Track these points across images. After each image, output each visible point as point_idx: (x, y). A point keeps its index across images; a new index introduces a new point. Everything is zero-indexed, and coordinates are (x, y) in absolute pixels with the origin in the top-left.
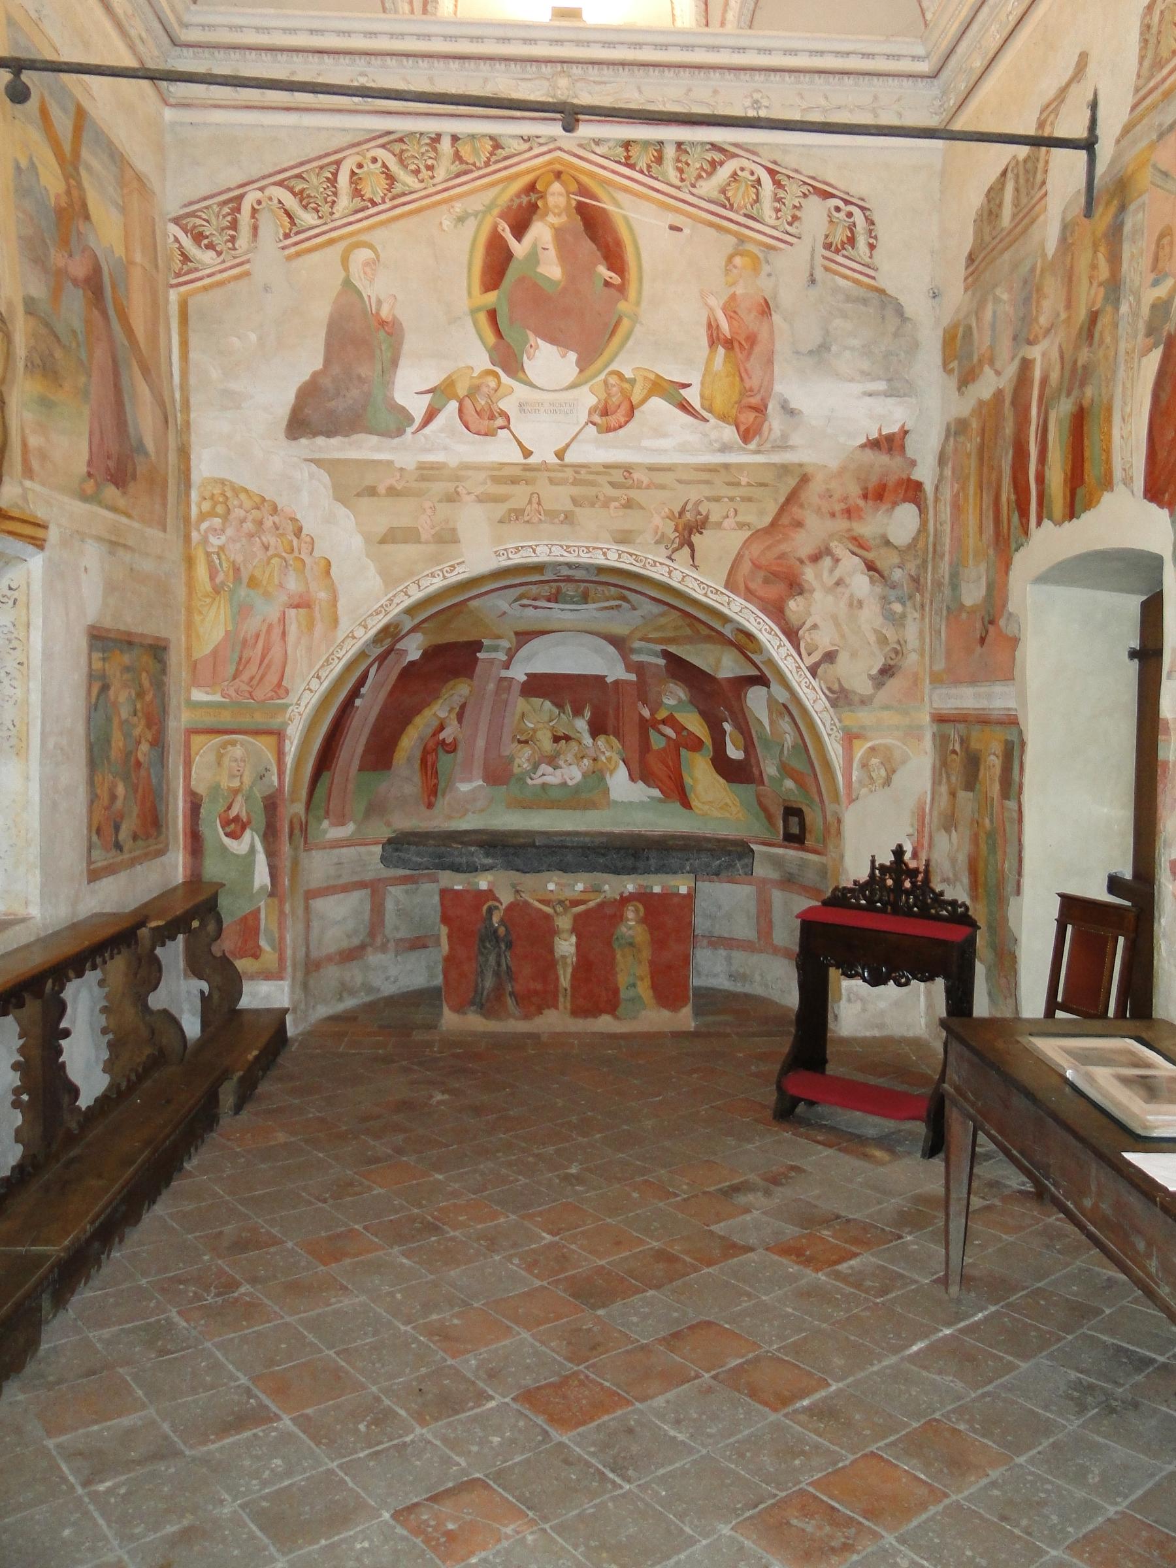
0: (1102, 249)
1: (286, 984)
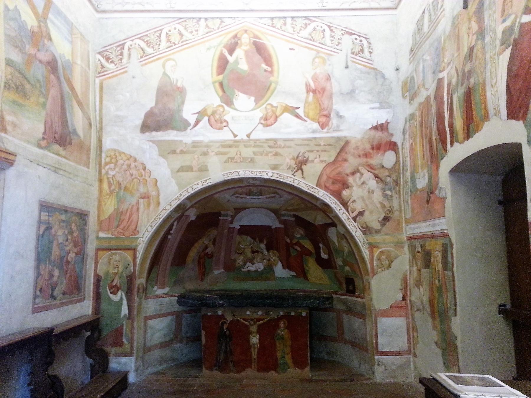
0: (473, 19)
1: (133, 358)
